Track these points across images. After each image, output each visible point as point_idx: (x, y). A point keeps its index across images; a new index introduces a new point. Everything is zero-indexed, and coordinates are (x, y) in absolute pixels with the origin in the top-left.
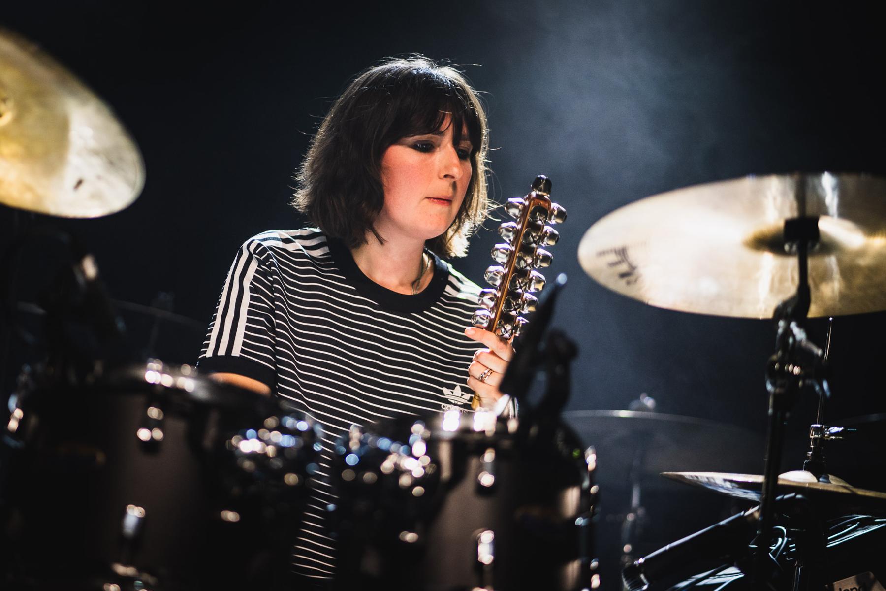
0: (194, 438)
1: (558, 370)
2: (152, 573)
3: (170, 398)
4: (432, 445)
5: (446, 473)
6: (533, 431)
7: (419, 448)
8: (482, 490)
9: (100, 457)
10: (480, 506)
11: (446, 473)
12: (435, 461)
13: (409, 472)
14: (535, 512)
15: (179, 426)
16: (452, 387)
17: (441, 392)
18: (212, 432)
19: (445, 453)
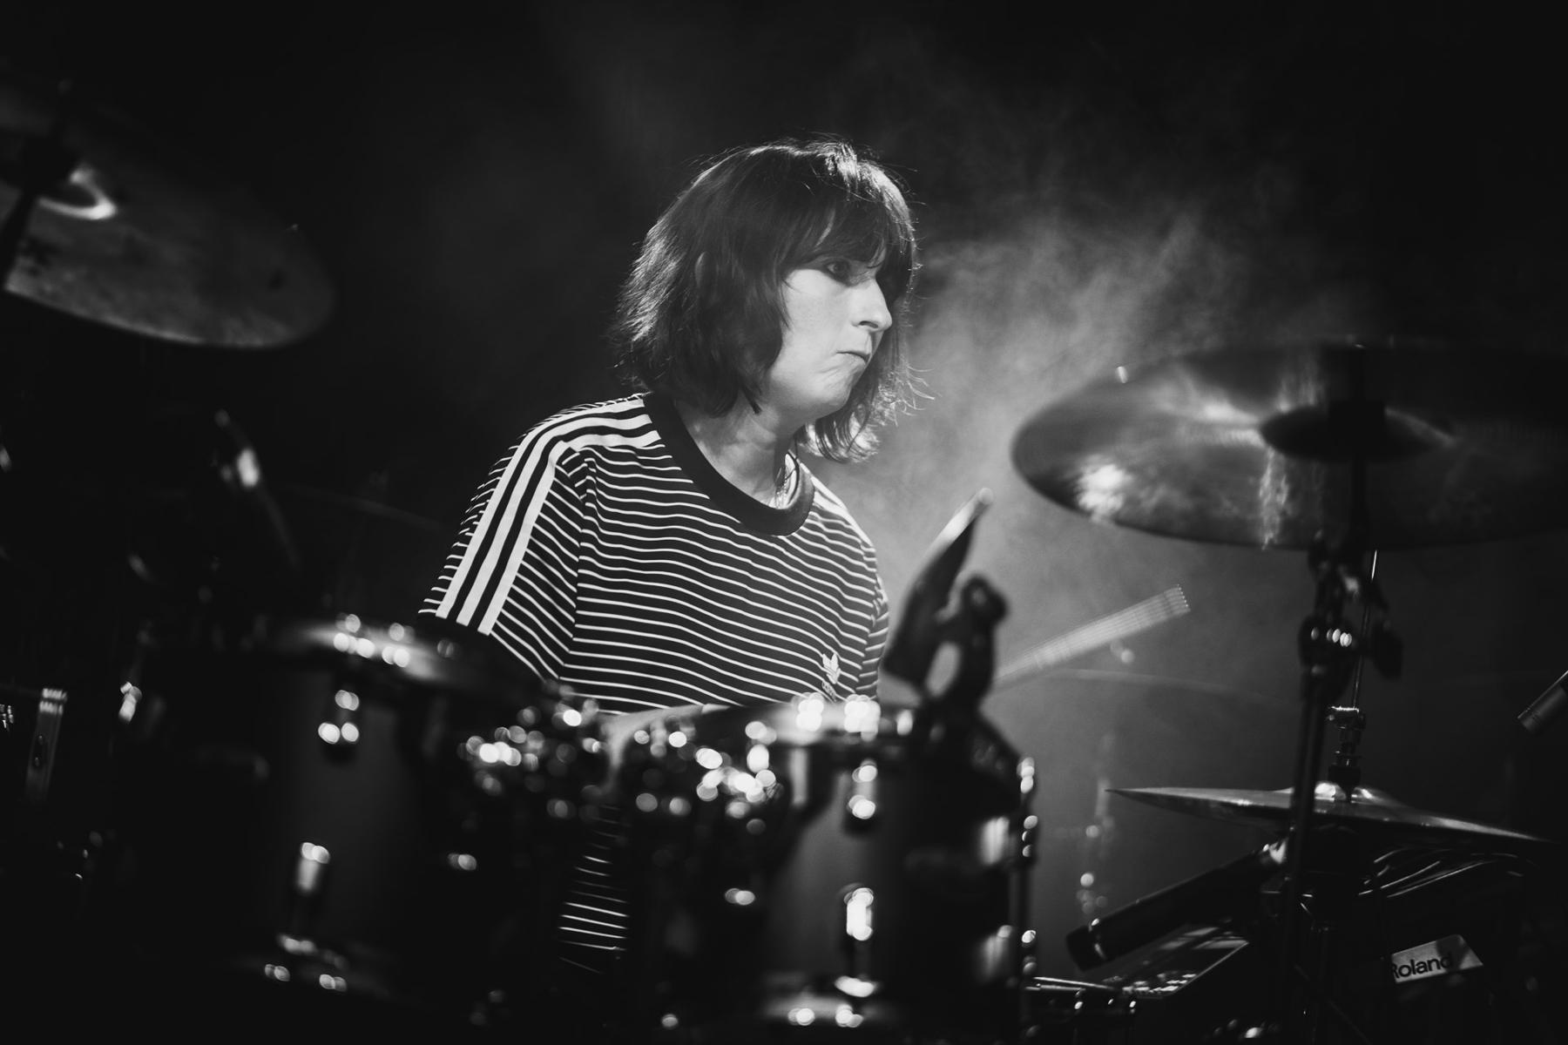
0: (407, 739)
1: (977, 641)
2: (339, 950)
3: (372, 677)
4: (779, 753)
5: (799, 797)
6: (936, 732)
7: (758, 758)
8: (854, 825)
9: (261, 767)
10: (851, 847)
11: (799, 797)
12: (784, 781)
13: (741, 796)
14: (937, 858)
15: (385, 719)
16: (830, 655)
17: (820, 660)
18: (435, 731)
19: (798, 767)
